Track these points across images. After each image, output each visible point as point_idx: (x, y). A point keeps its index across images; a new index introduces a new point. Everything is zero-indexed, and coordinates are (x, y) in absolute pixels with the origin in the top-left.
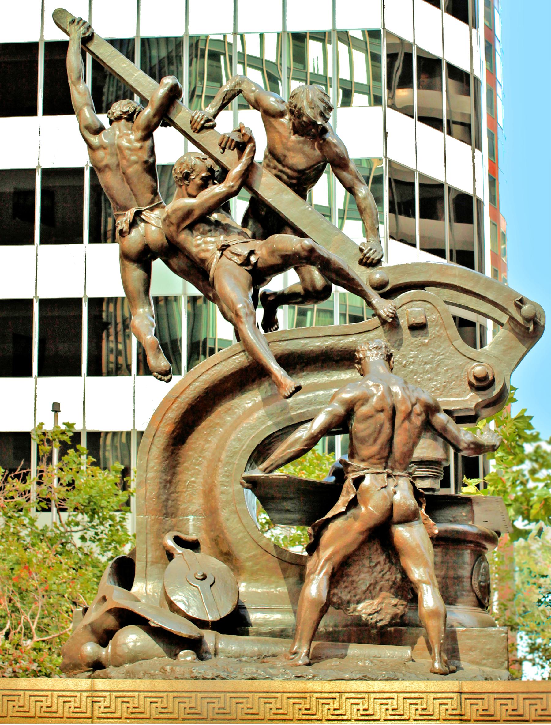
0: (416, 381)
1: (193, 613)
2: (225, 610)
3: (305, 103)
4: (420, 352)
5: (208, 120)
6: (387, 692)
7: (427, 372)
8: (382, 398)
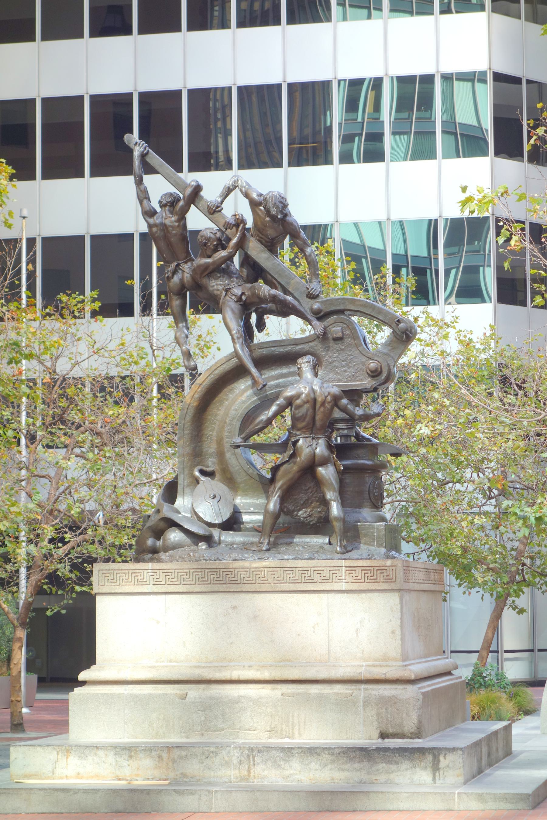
1: (208, 519)
2: (226, 515)
4: (340, 354)
5: (218, 207)
7: (344, 366)
8: (308, 395)
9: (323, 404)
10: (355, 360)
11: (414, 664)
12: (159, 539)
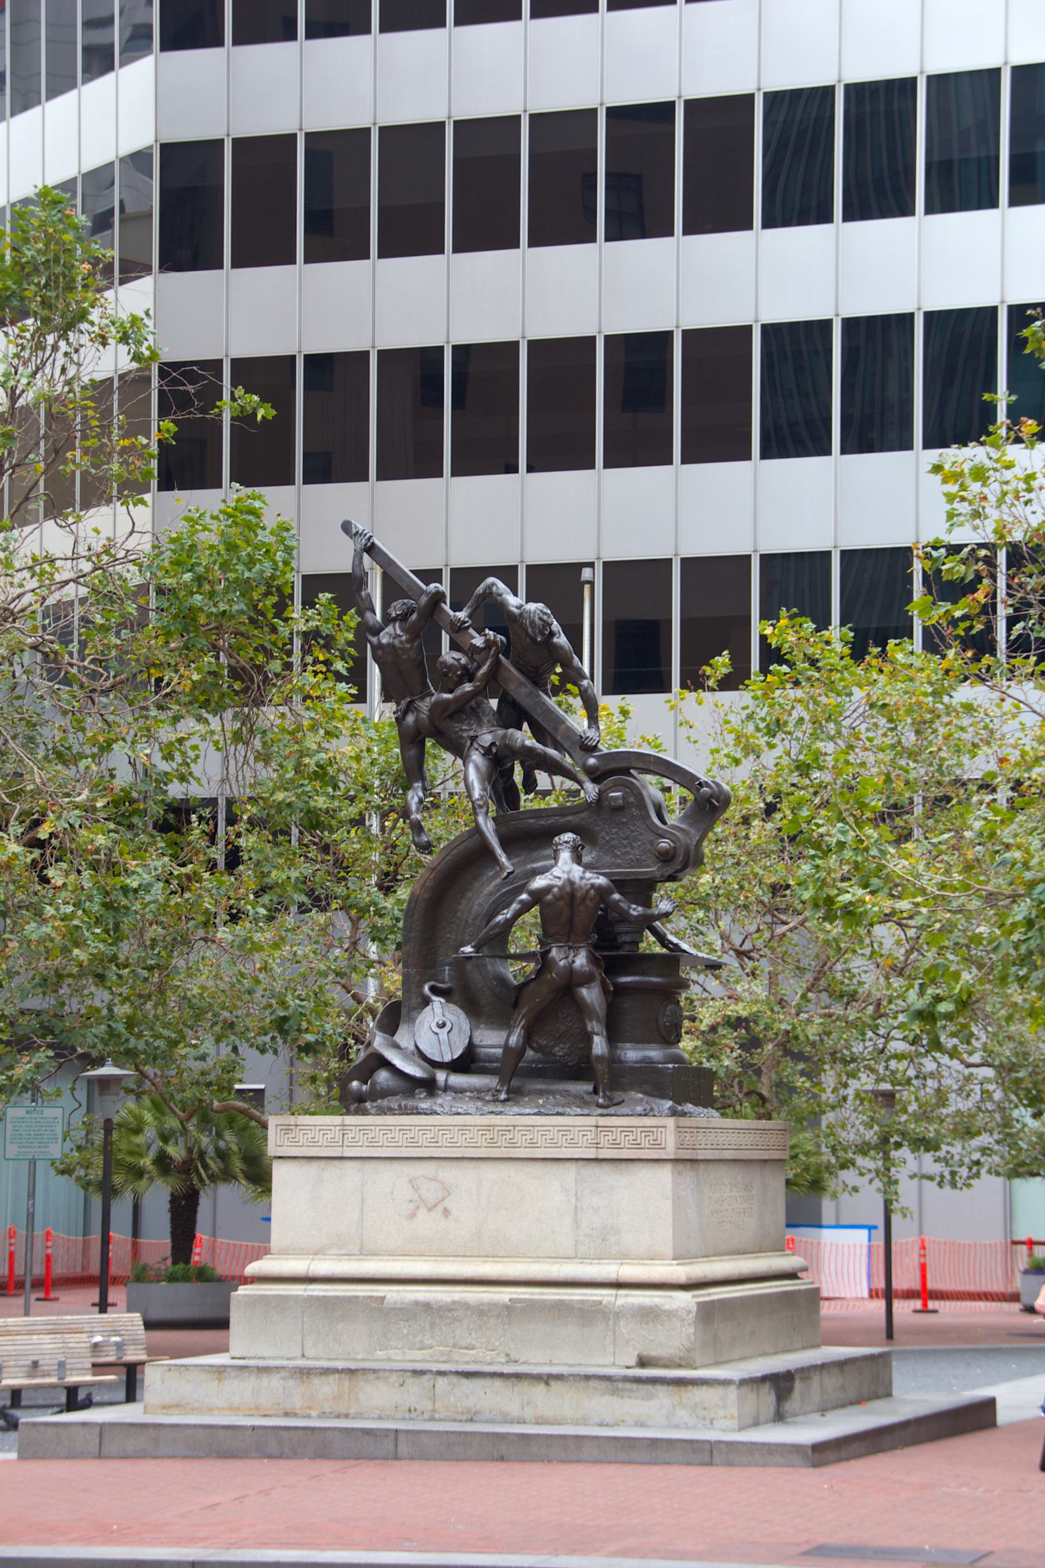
9: (584, 899)
11: (270, 1358)
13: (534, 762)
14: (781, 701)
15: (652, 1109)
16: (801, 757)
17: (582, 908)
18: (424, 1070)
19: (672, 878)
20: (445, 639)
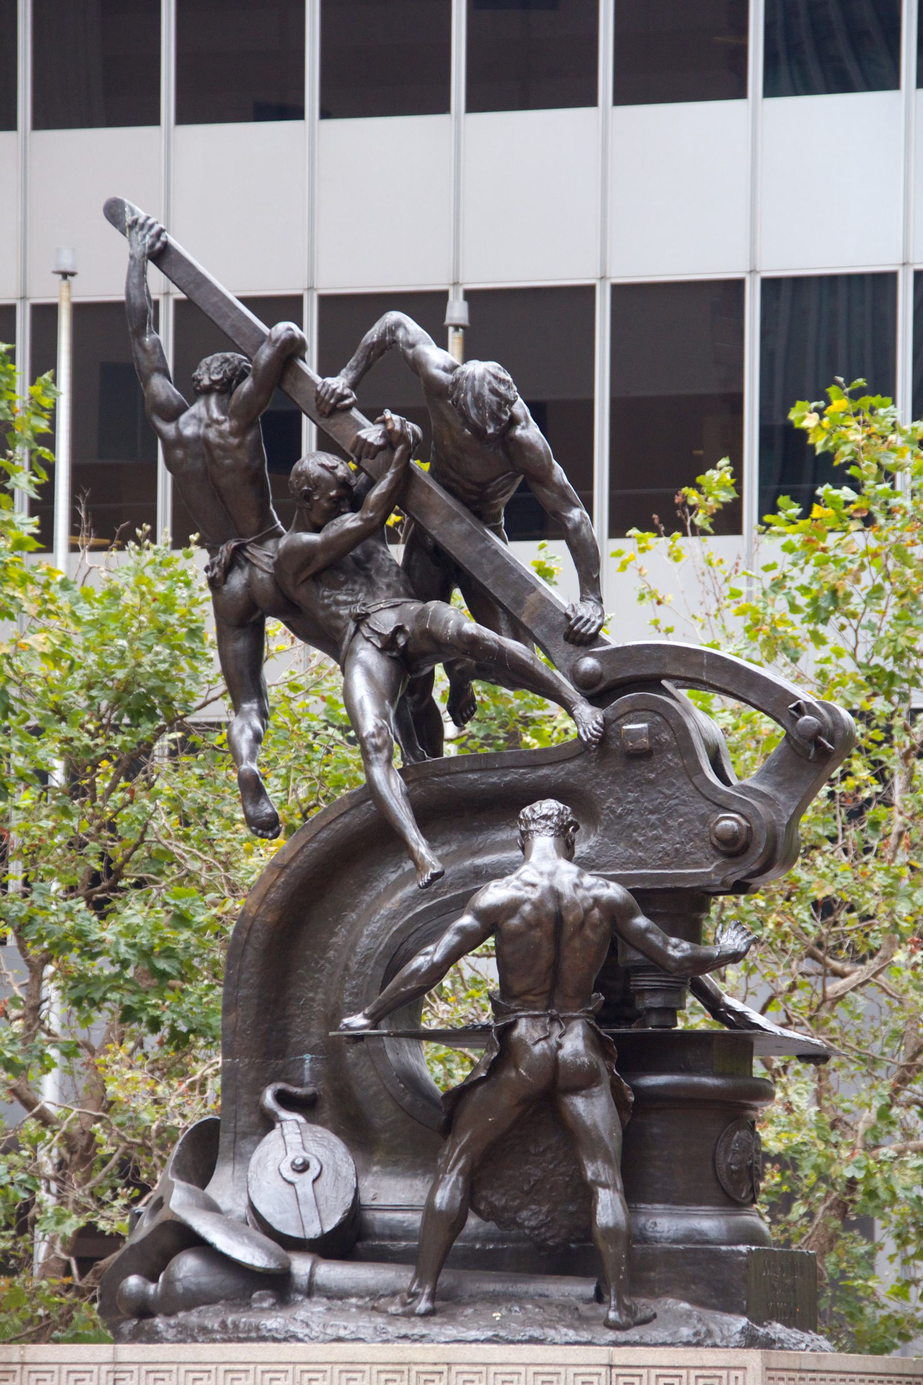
0: (636, 841)
3: (469, 397)
6: (512, 1364)
7: (653, 827)
9: (581, 926)
10: (683, 809)
12: (155, 1280)
13: (477, 663)
14: (840, 553)
15: (709, 1334)
16: (877, 660)
17: (577, 943)
18: (270, 1254)
19: (741, 888)
20: (309, 431)
